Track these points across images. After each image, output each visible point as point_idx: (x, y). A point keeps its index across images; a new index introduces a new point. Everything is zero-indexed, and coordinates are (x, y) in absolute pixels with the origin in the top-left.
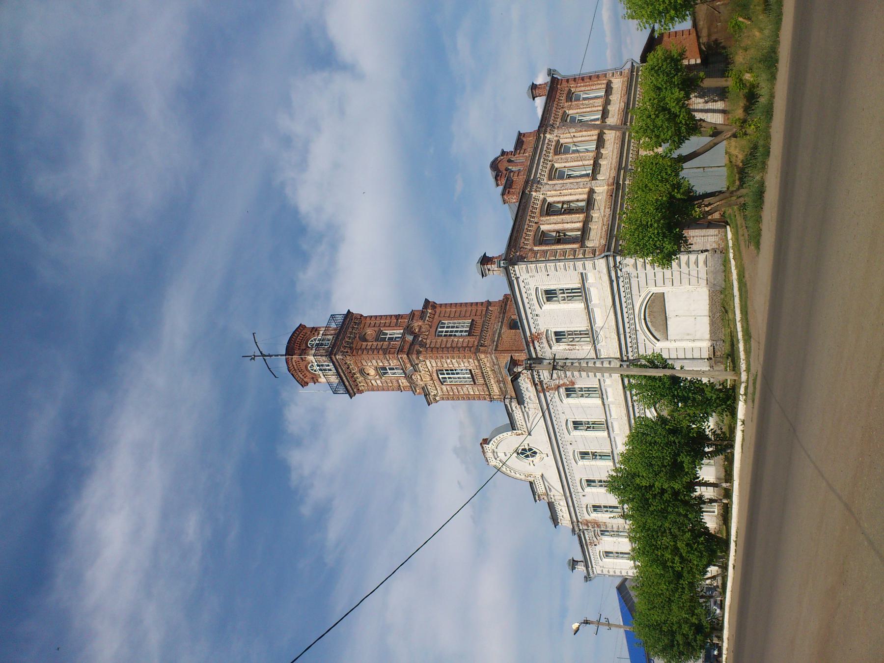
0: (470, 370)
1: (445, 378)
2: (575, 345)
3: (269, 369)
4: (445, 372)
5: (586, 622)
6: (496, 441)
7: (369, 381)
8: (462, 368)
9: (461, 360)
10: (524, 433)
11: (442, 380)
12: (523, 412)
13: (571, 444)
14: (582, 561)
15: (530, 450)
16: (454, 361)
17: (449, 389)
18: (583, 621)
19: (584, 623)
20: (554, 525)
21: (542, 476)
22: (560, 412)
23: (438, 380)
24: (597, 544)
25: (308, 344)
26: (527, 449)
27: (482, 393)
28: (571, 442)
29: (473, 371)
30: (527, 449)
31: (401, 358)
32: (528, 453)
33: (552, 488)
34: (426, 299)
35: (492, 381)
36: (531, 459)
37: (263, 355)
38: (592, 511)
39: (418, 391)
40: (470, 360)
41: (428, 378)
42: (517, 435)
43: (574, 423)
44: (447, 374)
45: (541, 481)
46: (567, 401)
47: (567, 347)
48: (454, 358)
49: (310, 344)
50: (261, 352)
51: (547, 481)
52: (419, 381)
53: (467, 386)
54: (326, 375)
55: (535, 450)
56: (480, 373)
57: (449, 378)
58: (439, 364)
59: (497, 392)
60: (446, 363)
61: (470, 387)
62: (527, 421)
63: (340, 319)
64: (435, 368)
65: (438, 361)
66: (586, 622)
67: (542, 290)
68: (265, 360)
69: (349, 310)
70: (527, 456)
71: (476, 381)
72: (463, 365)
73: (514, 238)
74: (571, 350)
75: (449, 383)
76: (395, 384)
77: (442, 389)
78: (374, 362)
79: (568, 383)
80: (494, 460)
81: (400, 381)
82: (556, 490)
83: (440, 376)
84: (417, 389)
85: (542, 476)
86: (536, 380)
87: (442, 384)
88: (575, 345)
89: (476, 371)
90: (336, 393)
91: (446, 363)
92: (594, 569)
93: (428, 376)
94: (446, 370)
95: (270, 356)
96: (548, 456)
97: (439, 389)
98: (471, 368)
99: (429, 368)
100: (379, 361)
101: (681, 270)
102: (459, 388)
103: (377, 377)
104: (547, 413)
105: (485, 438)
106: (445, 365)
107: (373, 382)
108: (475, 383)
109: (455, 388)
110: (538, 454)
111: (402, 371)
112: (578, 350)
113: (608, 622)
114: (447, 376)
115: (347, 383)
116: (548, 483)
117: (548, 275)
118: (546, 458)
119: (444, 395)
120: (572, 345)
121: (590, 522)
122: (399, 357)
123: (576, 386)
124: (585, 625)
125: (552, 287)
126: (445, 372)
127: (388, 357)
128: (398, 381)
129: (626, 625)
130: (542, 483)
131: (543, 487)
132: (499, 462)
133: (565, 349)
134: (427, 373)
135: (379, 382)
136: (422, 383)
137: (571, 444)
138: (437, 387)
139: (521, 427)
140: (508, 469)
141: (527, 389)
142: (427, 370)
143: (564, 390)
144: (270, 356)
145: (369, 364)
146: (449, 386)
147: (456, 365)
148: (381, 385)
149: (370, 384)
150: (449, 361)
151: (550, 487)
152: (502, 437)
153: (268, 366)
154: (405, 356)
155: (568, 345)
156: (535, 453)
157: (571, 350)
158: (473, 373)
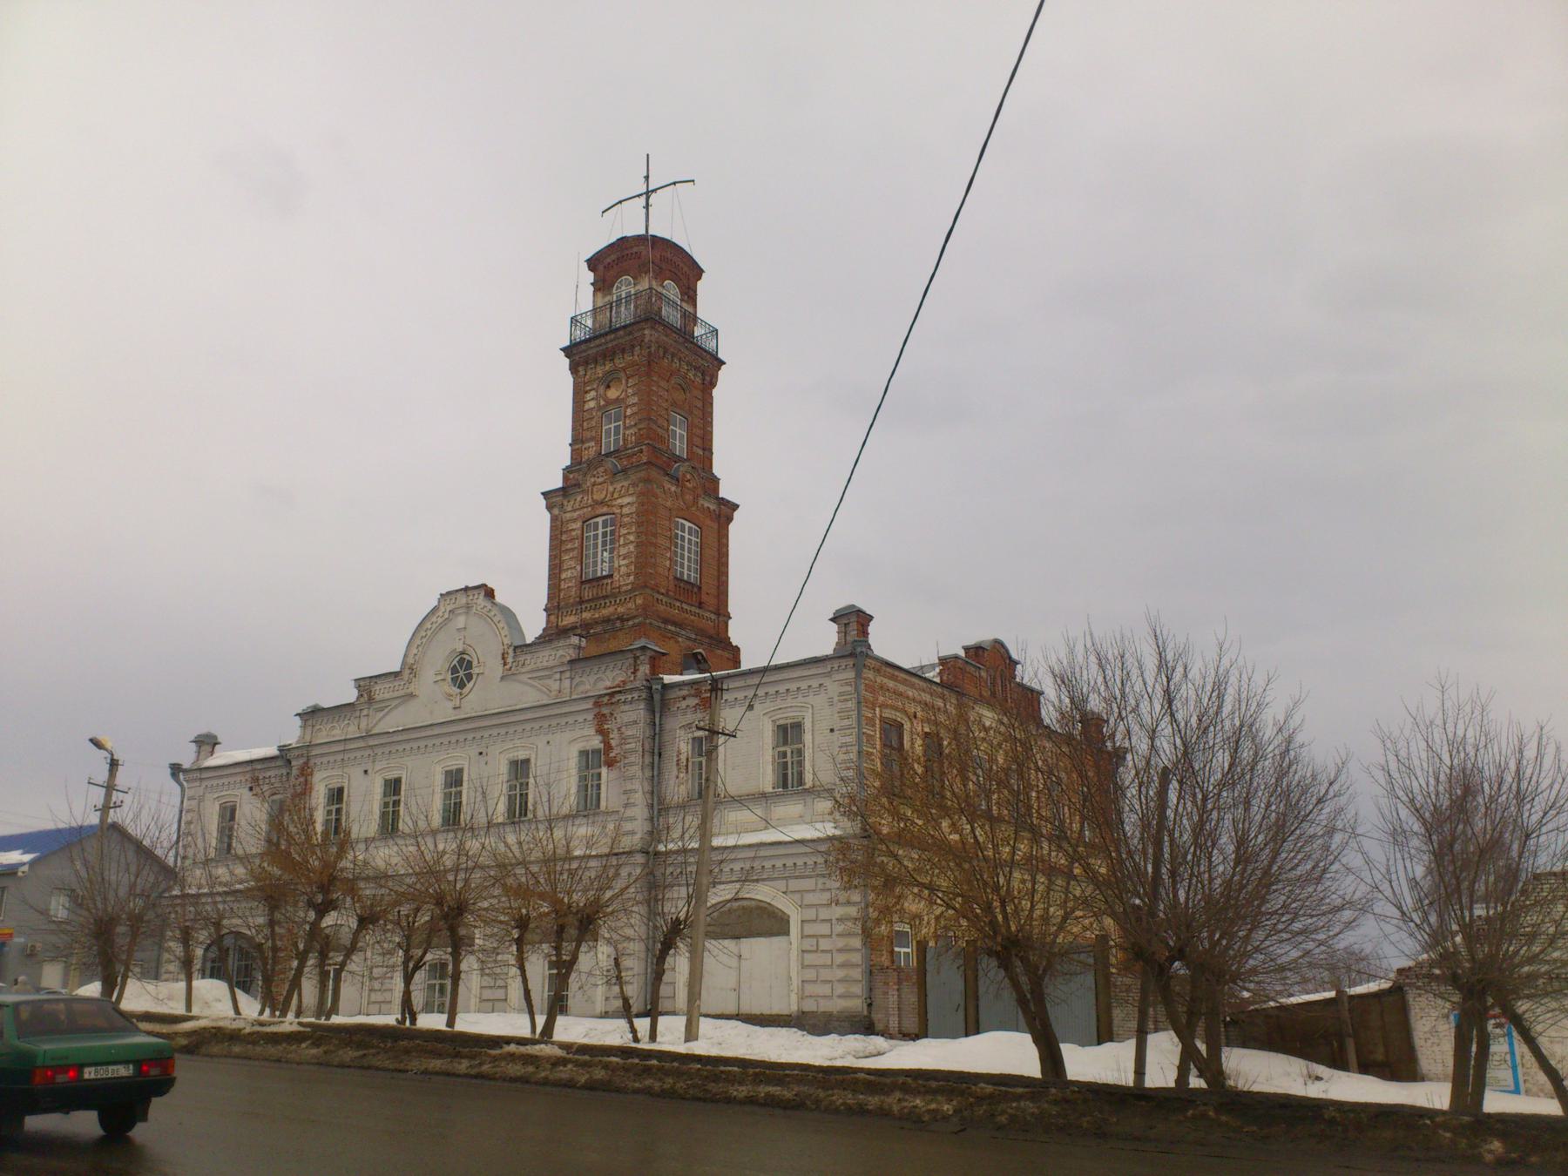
1: (596, 529)
2: (687, 772)
3: (620, 202)
4: (608, 529)
5: (114, 764)
6: (493, 613)
7: (595, 386)
9: (633, 560)
10: (507, 667)
11: (592, 521)
12: (552, 668)
13: (481, 753)
15: (469, 677)
16: (632, 548)
17: (574, 533)
18: (115, 757)
19: (112, 760)
20: (300, 712)
21: (412, 696)
22: (550, 737)
23: (593, 514)
24: (254, 792)
27: (562, 595)
28: (369, 772)
31: (641, 451)
32: (461, 673)
33: (383, 713)
34: (738, 506)
36: (449, 676)
37: (648, 194)
38: (331, 786)
39: (571, 476)
40: (632, 578)
41: (598, 496)
42: (503, 654)
43: (398, 781)
44: (605, 535)
45: (401, 693)
46: (574, 752)
47: (683, 757)
48: (637, 546)
50: (654, 191)
51: (400, 704)
52: (593, 480)
53: (579, 568)
55: (455, 662)
56: (604, 593)
57: (596, 537)
58: (626, 520)
59: (565, 623)
60: (629, 533)
61: (575, 573)
62: (534, 675)
63: (710, 345)
64: (619, 511)
66: (114, 764)
67: (800, 719)
68: (639, 196)
69: (724, 363)
70: (454, 670)
71: (587, 586)
72: (623, 562)
73: (896, 673)
75: (585, 535)
76: (588, 434)
77: (574, 520)
78: (635, 400)
79: (611, 755)
80: (449, 608)
81: (593, 444)
82: (380, 720)
83: (600, 520)
84: (576, 474)
85: (412, 696)
86: (623, 698)
87: (584, 522)
88: (687, 772)
89: (609, 588)
91: (629, 533)
92: (198, 784)
93: (603, 496)
94: (612, 533)
95: (647, 206)
96: (455, 708)
97: (575, 515)
99: (619, 501)
100: (635, 409)
101: (834, 997)
102: (575, 552)
103: (602, 403)
104: (545, 716)
105: (496, 594)
106: (624, 531)
107: (593, 394)
108: (582, 583)
109: (576, 545)
110: (459, 691)
112: (677, 777)
113: (112, 805)
114: (600, 531)
116: (396, 707)
117: (832, 730)
118: (451, 705)
119: (562, 523)
120: (687, 766)
121: (306, 781)
122: (644, 447)
123: (604, 770)
124: (109, 761)
126: (608, 529)
127: (641, 426)
128: (592, 439)
129: (1032, 690)
130: (396, 694)
131: (387, 696)
132: (446, 616)
133: (679, 753)
135: (592, 404)
136: (588, 484)
137: (366, 772)
138: (578, 513)
139: (521, 663)
140: (429, 633)
141: (600, 679)
142: (616, 496)
143: (597, 747)
144: (647, 206)
145: (630, 391)
146: (580, 536)
147: (623, 551)
148: (586, 407)
149: (588, 388)
150: (632, 538)
151: (386, 710)
152: (500, 625)
154: (645, 459)
155: (687, 759)
156: (462, 686)
157: (678, 765)
158: (605, 581)
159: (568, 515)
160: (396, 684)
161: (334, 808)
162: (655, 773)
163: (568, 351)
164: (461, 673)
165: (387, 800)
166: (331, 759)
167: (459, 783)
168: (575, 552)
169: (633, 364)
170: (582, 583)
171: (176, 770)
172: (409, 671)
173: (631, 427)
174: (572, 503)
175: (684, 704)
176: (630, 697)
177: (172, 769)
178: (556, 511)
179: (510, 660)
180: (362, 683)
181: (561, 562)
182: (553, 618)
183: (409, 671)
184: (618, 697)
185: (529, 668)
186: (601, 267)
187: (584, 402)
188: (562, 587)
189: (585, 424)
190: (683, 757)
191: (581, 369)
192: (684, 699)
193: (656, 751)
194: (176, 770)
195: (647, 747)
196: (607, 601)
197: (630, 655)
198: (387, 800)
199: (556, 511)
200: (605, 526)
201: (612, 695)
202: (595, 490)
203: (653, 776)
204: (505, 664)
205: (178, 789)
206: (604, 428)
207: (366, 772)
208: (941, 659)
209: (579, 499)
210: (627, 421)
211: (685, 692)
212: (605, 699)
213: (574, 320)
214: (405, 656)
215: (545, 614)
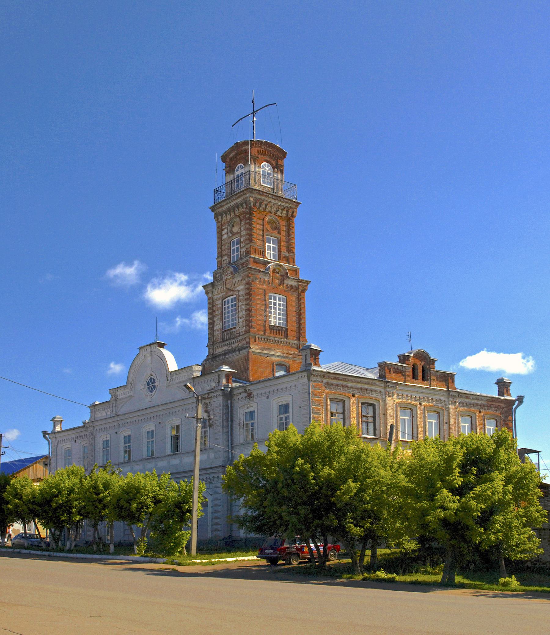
0: (235, 328)
4: (234, 303)
8: (237, 320)
10: (168, 382)
14: (61, 429)
17: (218, 306)
25: (265, 163)
26: (155, 384)
29: (235, 330)
30: (155, 384)
32: (151, 385)
35: (225, 348)
47: (241, 422)
49: (265, 165)
52: (226, 277)
53: (221, 324)
54: (232, 183)
55: (148, 380)
59: (216, 352)
65: (78, 508)
74: (239, 425)
83: (230, 298)
87: (223, 300)
90: (214, 192)
93: (231, 286)
98: (238, 329)
103: (230, 235)
110: (151, 393)
111: (236, 260)
115: (160, 408)
117: (300, 407)
120: (243, 425)
125: (290, 410)
126: (234, 303)
130: (126, 396)
131: (122, 397)
133: (240, 420)
134: (233, 285)
142: (236, 285)
147: (240, 314)
149: (224, 228)
150: (244, 307)
153: (244, 118)
155: (243, 422)
156: (151, 392)
157: (239, 425)
158: (233, 330)
159: (216, 297)
160: (126, 391)
161: (283, 416)
162: (229, 430)
163: (213, 209)
164: (151, 385)
165: (281, 416)
166: (177, 409)
167: (286, 411)
168: (219, 316)
169: (244, 213)
170: (223, 332)
171: (45, 434)
172: (130, 385)
173: (243, 247)
174: (217, 290)
175: (240, 397)
176: (216, 394)
177: (43, 433)
178: (210, 295)
179: (169, 378)
180: (112, 391)
181: (213, 322)
182: (211, 350)
183: (130, 385)
184: (211, 395)
185: (177, 381)
186: (228, 160)
187: (222, 235)
188: (215, 334)
189: (223, 247)
190: (241, 422)
191: (219, 217)
192: (240, 394)
193: (229, 419)
194: (45, 434)
195: (225, 418)
196: (234, 340)
197: (216, 374)
198: (281, 416)
199: (210, 295)
200: (232, 302)
201: (208, 394)
202: (227, 282)
203: (228, 431)
204: (167, 380)
205: (47, 442)
206: (232, 248)
207: (116, 433)
208: (378, 364)
209: (220, 288)
210: (242, 245)
211: (240, 391)
212: (206, 396)
213: (215, 191)
214: (128, 378)
215: (207, 348)
